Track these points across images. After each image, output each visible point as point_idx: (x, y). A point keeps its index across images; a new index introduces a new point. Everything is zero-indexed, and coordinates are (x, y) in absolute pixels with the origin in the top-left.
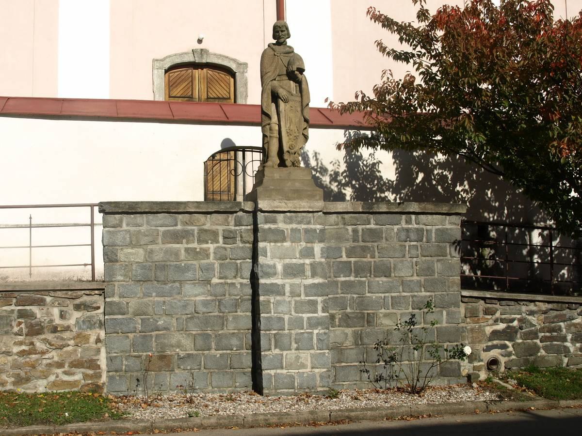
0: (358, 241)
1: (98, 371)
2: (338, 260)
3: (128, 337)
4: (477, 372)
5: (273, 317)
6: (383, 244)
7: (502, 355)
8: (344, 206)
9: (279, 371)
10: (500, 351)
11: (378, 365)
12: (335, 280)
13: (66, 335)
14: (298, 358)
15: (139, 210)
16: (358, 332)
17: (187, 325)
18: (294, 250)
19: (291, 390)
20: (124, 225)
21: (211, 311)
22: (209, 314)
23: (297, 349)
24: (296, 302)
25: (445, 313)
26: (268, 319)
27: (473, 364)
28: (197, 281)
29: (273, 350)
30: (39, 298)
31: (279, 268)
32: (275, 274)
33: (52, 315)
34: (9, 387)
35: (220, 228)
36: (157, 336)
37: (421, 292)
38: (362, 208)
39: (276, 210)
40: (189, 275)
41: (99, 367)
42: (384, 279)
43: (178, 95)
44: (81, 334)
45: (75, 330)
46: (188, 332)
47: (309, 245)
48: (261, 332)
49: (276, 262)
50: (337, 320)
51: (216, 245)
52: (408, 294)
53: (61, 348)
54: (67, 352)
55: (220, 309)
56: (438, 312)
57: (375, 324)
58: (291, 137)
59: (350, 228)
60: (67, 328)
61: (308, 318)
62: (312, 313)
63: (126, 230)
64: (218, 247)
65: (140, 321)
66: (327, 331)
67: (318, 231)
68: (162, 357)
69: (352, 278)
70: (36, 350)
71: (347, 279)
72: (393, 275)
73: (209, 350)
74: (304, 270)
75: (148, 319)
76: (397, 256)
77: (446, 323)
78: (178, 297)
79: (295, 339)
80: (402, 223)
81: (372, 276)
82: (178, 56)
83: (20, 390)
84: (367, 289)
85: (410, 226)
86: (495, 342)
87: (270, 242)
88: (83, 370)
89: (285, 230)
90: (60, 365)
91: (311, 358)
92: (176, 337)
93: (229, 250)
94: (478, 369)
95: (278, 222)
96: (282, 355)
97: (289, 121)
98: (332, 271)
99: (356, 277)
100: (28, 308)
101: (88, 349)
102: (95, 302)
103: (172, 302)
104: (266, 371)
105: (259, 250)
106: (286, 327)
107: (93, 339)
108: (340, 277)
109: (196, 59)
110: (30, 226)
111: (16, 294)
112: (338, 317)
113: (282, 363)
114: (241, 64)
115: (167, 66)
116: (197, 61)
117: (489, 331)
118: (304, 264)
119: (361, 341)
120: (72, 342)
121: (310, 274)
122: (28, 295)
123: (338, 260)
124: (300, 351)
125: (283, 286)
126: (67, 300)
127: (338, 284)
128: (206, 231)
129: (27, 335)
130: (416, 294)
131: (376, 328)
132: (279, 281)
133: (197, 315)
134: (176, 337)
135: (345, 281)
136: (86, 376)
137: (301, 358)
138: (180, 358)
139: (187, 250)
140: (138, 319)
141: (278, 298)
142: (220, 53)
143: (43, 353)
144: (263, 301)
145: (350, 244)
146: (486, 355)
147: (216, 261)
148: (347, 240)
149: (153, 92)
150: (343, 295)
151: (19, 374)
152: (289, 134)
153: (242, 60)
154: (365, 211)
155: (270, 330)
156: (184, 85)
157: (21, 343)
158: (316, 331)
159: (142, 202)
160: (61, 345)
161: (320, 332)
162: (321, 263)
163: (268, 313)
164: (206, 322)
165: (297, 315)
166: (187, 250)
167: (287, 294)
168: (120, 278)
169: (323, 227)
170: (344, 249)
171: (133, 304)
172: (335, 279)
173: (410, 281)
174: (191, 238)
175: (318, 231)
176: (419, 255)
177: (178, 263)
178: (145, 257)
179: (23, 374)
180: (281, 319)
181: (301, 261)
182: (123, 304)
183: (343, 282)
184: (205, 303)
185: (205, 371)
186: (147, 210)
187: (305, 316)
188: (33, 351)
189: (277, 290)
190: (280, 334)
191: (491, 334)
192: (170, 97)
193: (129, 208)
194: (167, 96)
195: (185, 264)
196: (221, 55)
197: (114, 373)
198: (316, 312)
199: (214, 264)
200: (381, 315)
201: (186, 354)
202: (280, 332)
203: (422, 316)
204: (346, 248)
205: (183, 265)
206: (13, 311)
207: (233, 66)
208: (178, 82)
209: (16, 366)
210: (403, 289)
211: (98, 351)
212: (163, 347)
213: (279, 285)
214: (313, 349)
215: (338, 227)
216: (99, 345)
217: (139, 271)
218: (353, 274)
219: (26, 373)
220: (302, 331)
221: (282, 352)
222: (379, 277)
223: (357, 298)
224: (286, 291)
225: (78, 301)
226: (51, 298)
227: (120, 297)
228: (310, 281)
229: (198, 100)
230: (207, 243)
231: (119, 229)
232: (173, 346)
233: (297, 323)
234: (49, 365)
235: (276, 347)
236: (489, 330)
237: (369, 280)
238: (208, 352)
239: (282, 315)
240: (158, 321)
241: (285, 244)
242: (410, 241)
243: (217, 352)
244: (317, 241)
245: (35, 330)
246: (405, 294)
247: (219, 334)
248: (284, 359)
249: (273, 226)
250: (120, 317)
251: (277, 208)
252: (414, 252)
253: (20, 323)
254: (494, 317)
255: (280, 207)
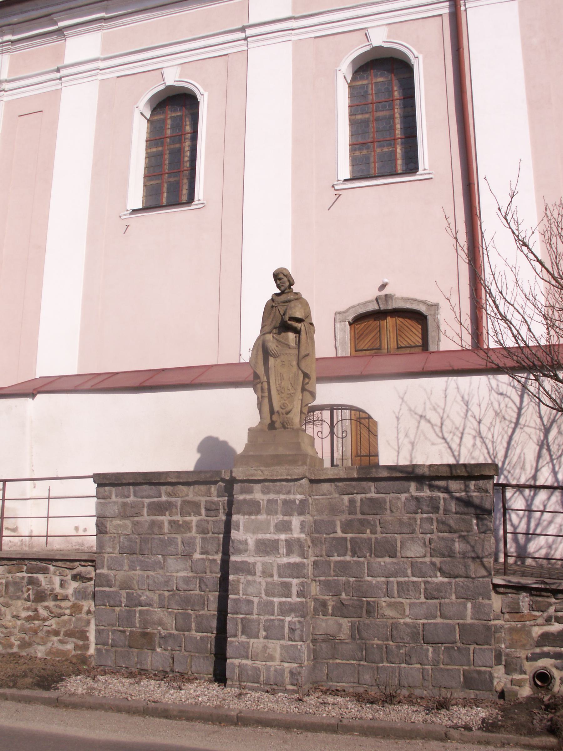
0: (355, 514)
1: (86, 642)
2: (332, 535)
3: (114, 610)
4: (517, 688)
5: (241, 599)
6: (388, 516)
7: (557, 668)
8: (336, 472)
9: (244, 661)
10: (552, 661)
11: (382, 667)
12: (328, 559)
13: (64, 604)
14: (265, 647)
15: (124, 481)
16: (355, 623)
17: (169, 603)
18: (268, 523)
19: (256, 685)
20: (114, 496)
21: (192, 589)
22: (191, 592)
23: (266, 637)
24: (267, 584)
25: (469, 605)
26: (237, 601)
27: (511, 677)
28: (180, 556)
29: (239, 637)
30: (43, 566)
31: (251, 543)
32: (246, 550)
33: (53, 584)
34: (15, 650)
35: (203, 500)
36: (140, 612)
37: (436, 577)
38: (357, 474)
39: (250, 478)
40: (171, 549)
41: (87, 638)
42: (387, 560)
43: (366, 348)
44: (76, 603)
45: (72, 599)
46: (170, 610)
47: (286, 518)
48: (229, 615)
49: (248, 537)
50: (330, 608)
51: (198, 518)
52: (420, 579)
53: (59, 616)
54: (63, 621)
55: (201, 588)
56: (460, 603)
57: (376, 615)
58: (283, 395)
59: (346, 498)
60: (65, 598)
61: (280, 603)
62: (285, 597)
63: (114, 502)
64: (201, 520)
65: (125, 595)
66: (302, 620)
67: (297, 502)
68: (145, 635)
69: (348, 558)
70: (39, 616)
71: (342, 558)
72: (398, 554)
73: (189, 632)
74: (278, 547)
75: (133, 594)
76: (405, 531)
77: (472, 619)
78: (161, 572)
79: (264, 626)
80: (411, 490)
81: (373, 555)
82: (362, 306)
83: (24, 654)
84: (366, 571)
85: (422, 494)
86: (546, 649)
87: (244, 514)
88: (74, 640)
89: (261, 502)
90: (57, 633)
91: (281, 648)
92: (158, 613)
93: (211, 523)
94: (520, 684)
95: (255, 491)
96: (248, 643)
97: (279, 378)
98: (324, 549)
99: (353, 556)
100: (35, 575)
101: (79, 620)
102: (89, 573)
103: (154, 577)
104: (230, 660)
105: (232, 523)
106: (255, 611)
107: (85, 609)
108: (333, 556)
109: (381, 306)
110: (49, 498)
111: (27, 562)
112: (331, 604)
113: (247, 652)
114: (432, 306)
115: (350, 318)
116: (382, 309)
117: (537, 633)
118: (278, 540)
119: (359, 635)
120: (68, 612)
121: (285, 551)
122: (35, 563)
123: (332, 535)
124: (269, 640)
125: (254, 564)
126: (66, 569)
127: (330, 565)
128: (189, 502)
129: (33, 602)
130: (429, 579)
131: (378, 620)
132: (251, 560)
133: (179, 592)
134: (158, 613)
135: (340, 562)
136: (77, 647)
137: (270, 648)
138: (162, 637)
139: (170, 522)
140: (123, 593)
141: (250, 578)
142: (407, 296)
143: (45, 620)
144: (233, 581)
145: (345, 517)
146: (531, 666)
147: (198, 535)
148: (343, 512)
149: (336, 347)
150: (336, 578)
151: (24, 638)
152: (279, 392)
153: (432, 300)
154: (361, 476)
155: (237, 613)
156: (373, 334)
157: (28, 609)
158: (288, 619)
159: (127, 473)
160: (60, 614)
161: (293, 620)
162: (299, 540)
163: (236, 594)
164: (186, 602)
165: (268, 598)
166: (170, 522)
167: (258, 573)
168: (109, 550)
169: (304, 496)
170: (338, 523)
171: (120, 575)
172: (328, 559)
173: (421, 563)
174: (174, 510)
175: (297, 502)
176: (435, 530)
177: (161, 536)
178: (131, 529)
179: (27, 638)
180: (250, 602)
181: (276, 537)
182: (111, 576)
183: (336, 562)
184: (187, 580)
185: (185, 653)
186: (131, 481)
187: (276, 600)
188: (36, 617)
189: (247, 569)
190: (248, 619)
191: (539, 637)
192: (356, 351)
193: (178, 477)
194: (353, 350)
195: (168, 538)
196: (408, 299)
197: (101, 646)
198: (289, 595)
199: (195, 538)
200: (384, 604)
201: (168, 633)
202: (247, 616)
203: (439, 608)
204: (341, 521)
205: (166, 538)
206: (23, 578)
207: (423, 309)
208: (365, 333)
209: (23, 631)
210: (412, 573)
211: (88, 623)
212: (145, 623)
213: (250, 563)
214: (283, 638)
215: (331, 496)
216: (90, 616)
217: (126, 544)
218: (349, 553)
219: (30, 637)
220: (272, 617)
221: (248, 640)
222: (382, 557)
223: (353, 582)
224: (257, 570)
225: (74, 572)
226: (54, 567)
227: (108, 569)
228: (285, 560)
229: (386, 351)
230: (190, 515)
231: (109, 500)
232: (155, 624)
233: (267, 608)
234: (48, 632)
235: (243, 633)
236: (537, 631)
237: (368, 561)
238: (188, 633)
239: (251, 598)
240: (140, 596)
241: (259, 517)
242: (421, 513)
243: (198, 634)
244: (296, 514)
245: (40, 597)
246: (415, 579)
247: (200, 615)
248: (251, 648)
249: (248, 497)
250: (107, 589)
251: (252, 475)
252: (426, 526)
253: (29, 590)
254: (545, 615)
255: (255, 476)
